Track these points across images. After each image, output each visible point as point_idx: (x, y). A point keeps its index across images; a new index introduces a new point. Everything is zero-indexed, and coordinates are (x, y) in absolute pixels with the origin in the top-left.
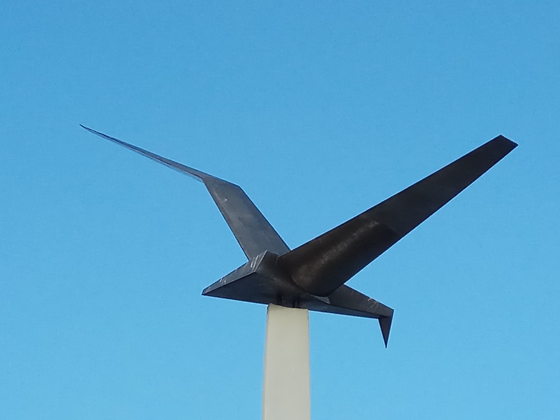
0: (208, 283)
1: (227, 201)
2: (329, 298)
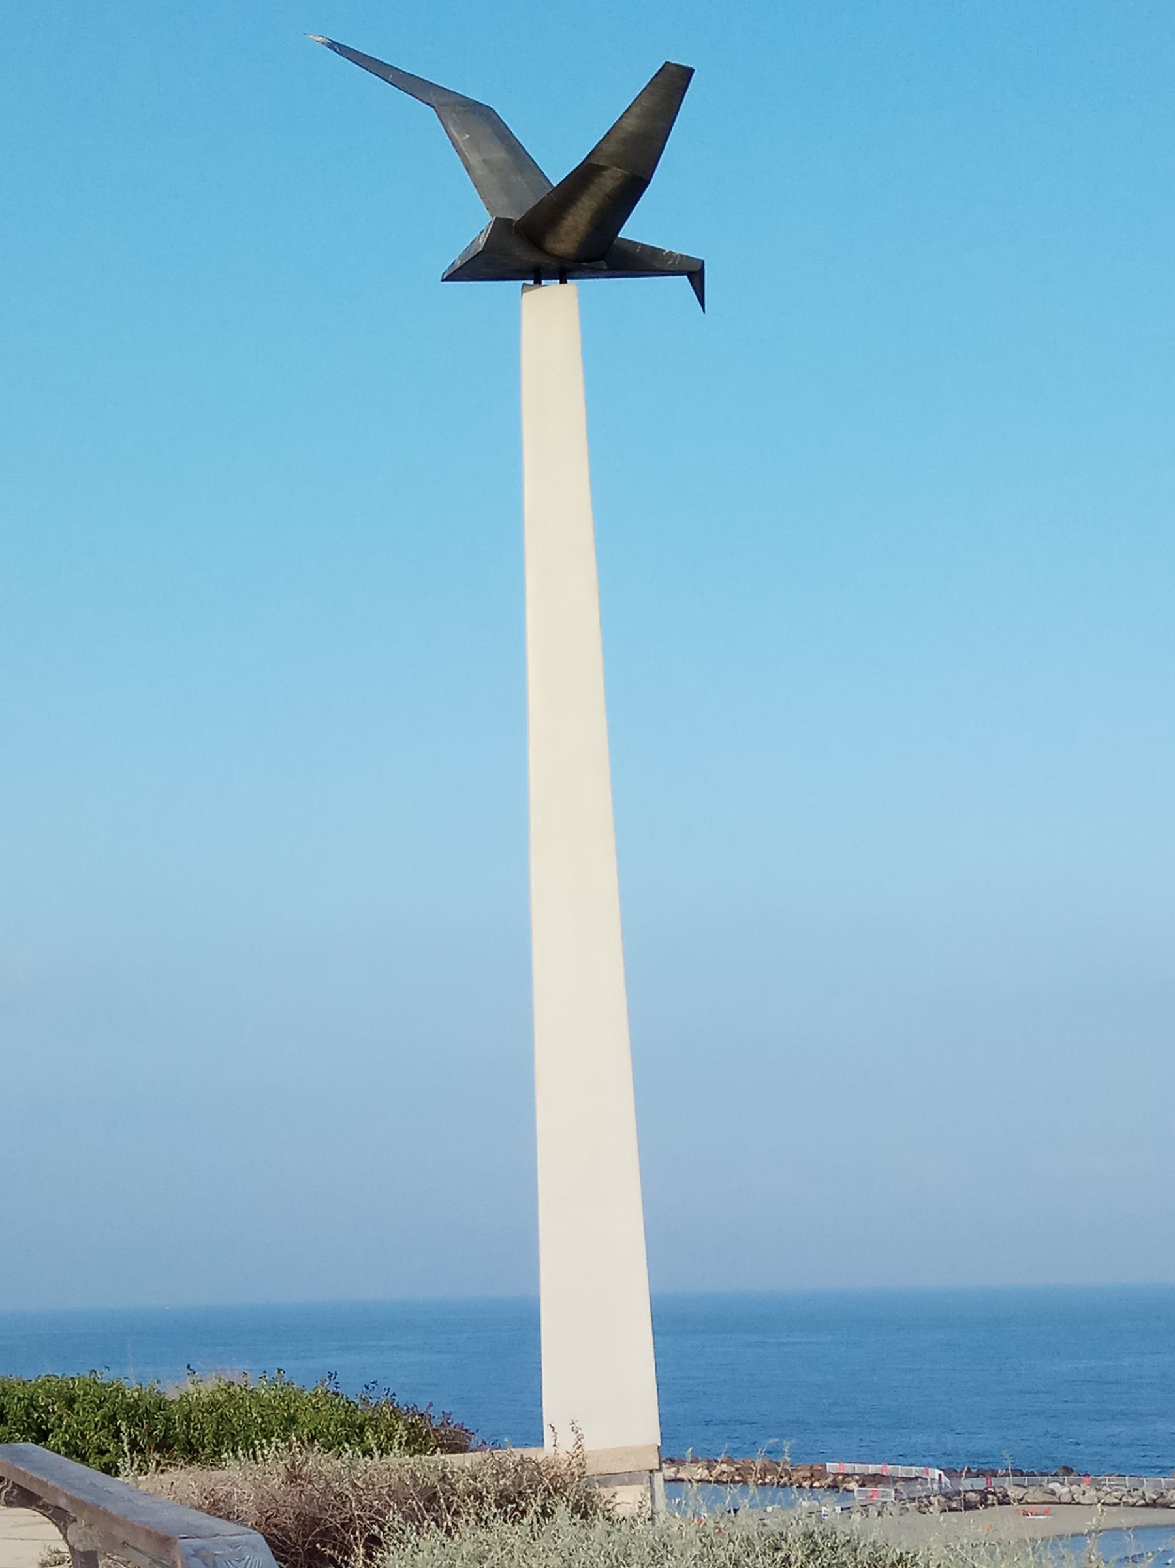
0: (444, 267)
1: (469, 137)
2: (605, 261)
